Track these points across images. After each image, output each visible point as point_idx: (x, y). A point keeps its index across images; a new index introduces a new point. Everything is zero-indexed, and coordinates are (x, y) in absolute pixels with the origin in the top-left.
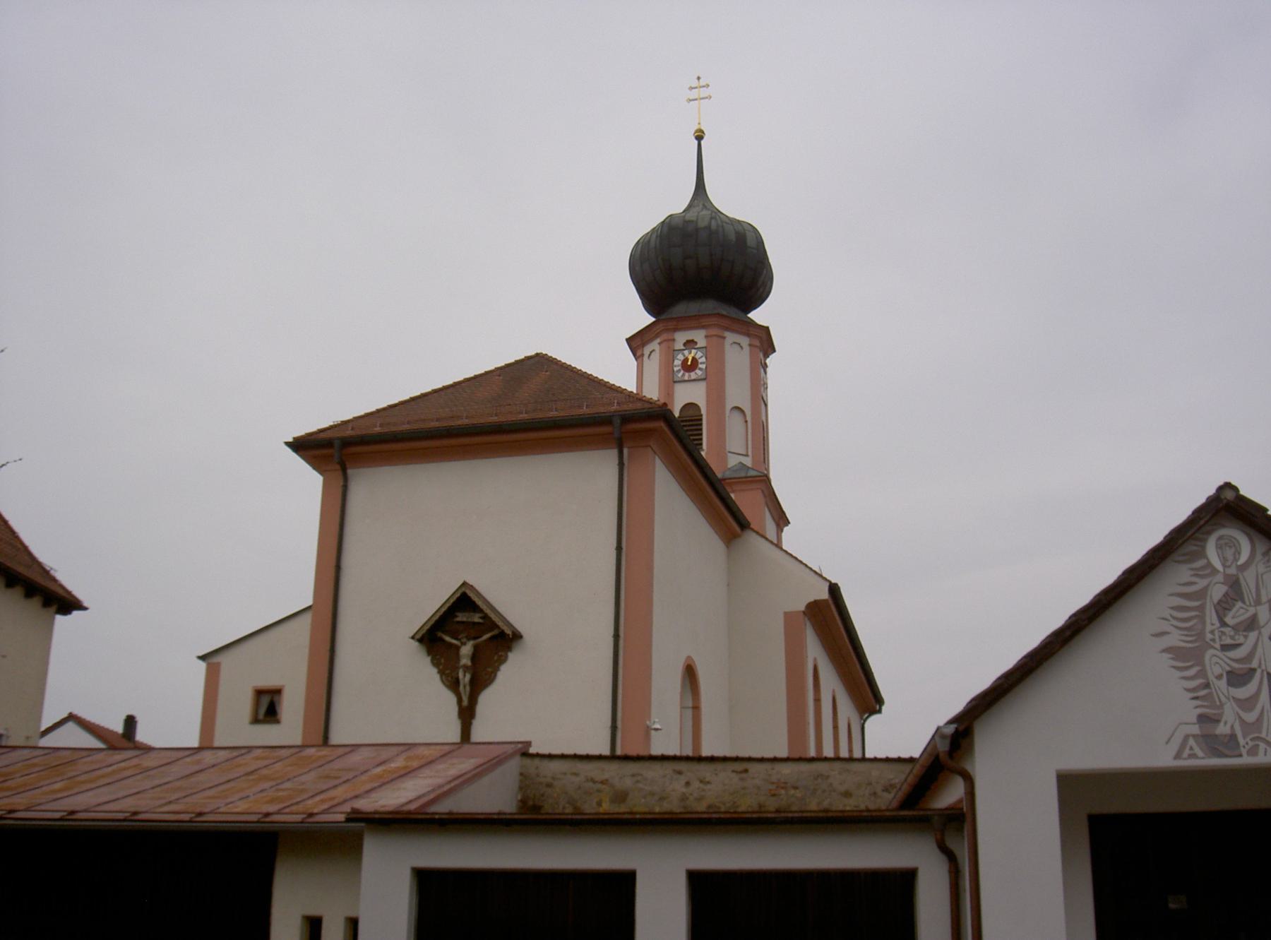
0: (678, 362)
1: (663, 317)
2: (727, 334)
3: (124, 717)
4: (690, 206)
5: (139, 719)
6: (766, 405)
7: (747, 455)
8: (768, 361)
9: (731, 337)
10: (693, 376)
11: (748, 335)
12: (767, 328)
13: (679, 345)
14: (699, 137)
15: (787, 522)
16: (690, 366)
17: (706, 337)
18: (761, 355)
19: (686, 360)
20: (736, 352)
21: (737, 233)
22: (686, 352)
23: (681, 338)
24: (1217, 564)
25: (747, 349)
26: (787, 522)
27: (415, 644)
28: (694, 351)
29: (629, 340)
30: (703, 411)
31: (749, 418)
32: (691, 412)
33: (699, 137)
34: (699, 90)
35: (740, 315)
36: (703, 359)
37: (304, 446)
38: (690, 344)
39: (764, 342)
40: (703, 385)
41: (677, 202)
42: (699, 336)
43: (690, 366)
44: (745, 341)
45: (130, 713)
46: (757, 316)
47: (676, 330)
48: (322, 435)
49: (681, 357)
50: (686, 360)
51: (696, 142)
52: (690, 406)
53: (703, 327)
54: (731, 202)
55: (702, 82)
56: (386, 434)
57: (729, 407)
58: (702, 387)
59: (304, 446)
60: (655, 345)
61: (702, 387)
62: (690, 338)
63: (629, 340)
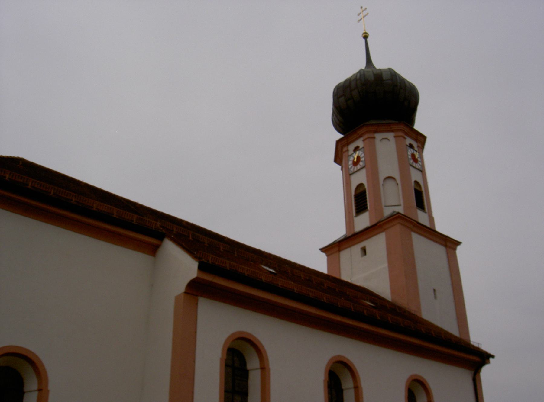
0: (350, 163)
5: (462, 245)
9: (379, 136)
10: (359, 167)
13: (351, 152)
14: (366, 37)
17: (363, 141)
20: (386, 146)
21: (374, 75)
23: (351, 147)
24: (52, 191)
30: (366, 187)
32: (361, 190)
33: (366, 37)
34: (363, 12)
37: (323, 250)
38: (356, 149)
39: (421, 139)
40: (364, 171)
41: (354, 66)
42: (360, 143)
43: (355, 164)
49: (352, 159)
51: (364, 40)
53: (392, 131)
55: (363, 9)
57: (382, 176)
58: (363, 172)
59: (323, 250)
61: (363, 172)
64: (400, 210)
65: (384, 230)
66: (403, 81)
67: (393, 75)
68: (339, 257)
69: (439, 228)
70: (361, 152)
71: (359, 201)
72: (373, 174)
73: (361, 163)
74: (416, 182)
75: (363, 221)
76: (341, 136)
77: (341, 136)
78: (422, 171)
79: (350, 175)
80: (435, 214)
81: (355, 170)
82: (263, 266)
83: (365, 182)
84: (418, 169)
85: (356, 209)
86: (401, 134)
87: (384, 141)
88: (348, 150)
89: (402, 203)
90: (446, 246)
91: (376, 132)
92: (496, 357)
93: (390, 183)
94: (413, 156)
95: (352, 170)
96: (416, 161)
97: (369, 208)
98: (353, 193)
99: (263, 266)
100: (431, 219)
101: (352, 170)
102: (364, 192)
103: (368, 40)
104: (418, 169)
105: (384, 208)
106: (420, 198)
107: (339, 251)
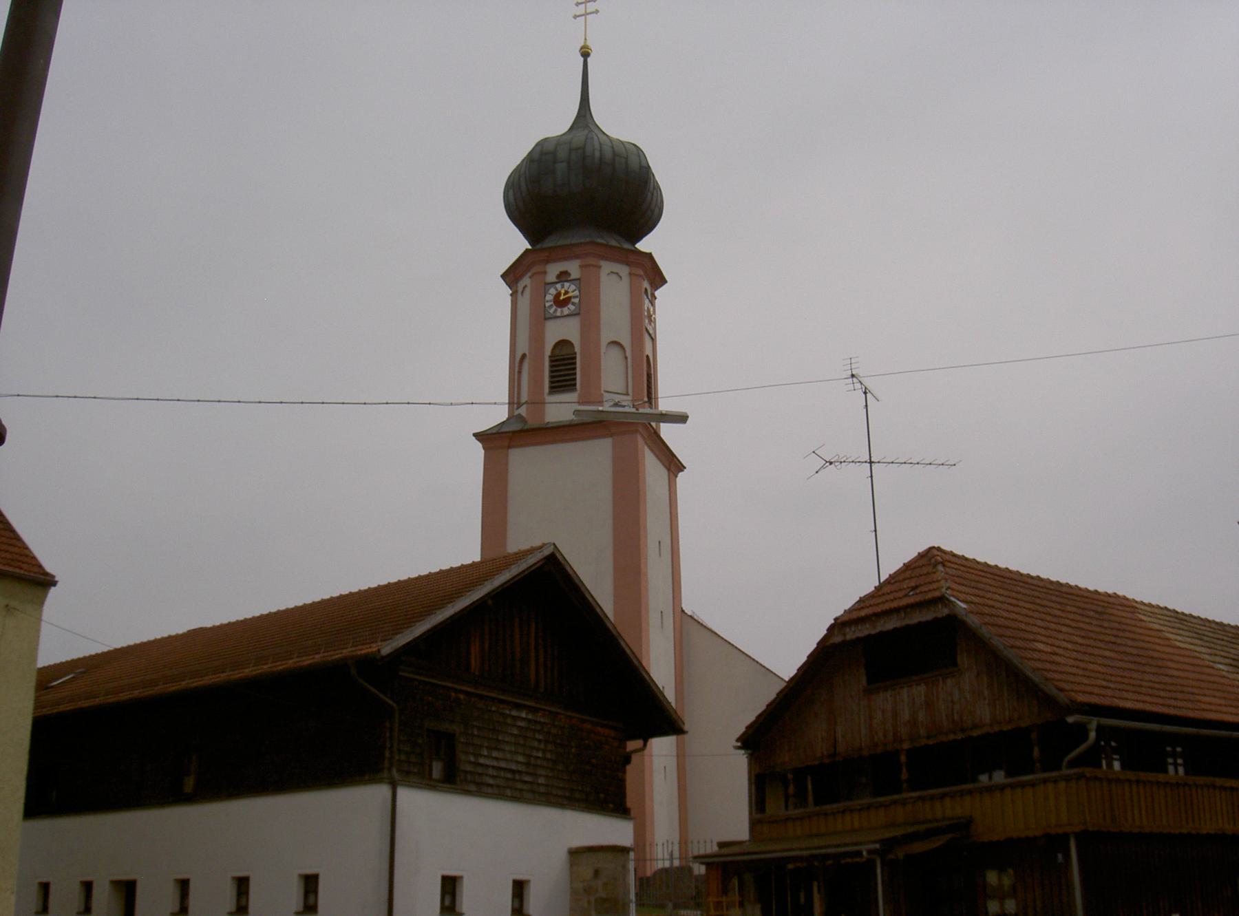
0: (549, 297)
1: (538, 246)
2: (603, 263)
3: (566, 850)
4: (572, 128)
6: (653, 340)
7: (627, 394)
8: (657, 293)
9: (607, 267)
10: (566, 311)
11: (628, 263)
12: (650, 254)
14: (585, 54)
15: (680, 467)
16: (560, 302)
17: (581, 267)
18: (646, 284)
19: (559, 294)
20: (613, 286)
22: (559, 286)
23: (553, 271)
26: (680, 467)
27: (686, 728)
28: (566, 285)
29: (504, 276)
30: (577, 349)
31: (629, 354)
33: (585, 54)
35: (627, 246)
36: (577, 293)
37: (479, 436)
38: (563, 276)
41: (556, 122)
42: (574, 268)
43: (560, 302)
44: (624, 270)
46: (643, 245)
47: (548, 261)
49: (553, 291)
50: (559, 294)
52: (563, 344)
53: (577, 257)
54: (617, 123)
59: (479, 436)
60: (526, 281)
61: (574, 323)
63: (504, 276)
65: (611, 435)
68: (507, 455)
71: (563, 370)
73: (572, 307)
75: (561, 408)
79: (546, 319)
81: (558, 314)
82: (809, 778)
87: (614, 276)
88: (545, 273)
90: (669, 470)
93: (615, 353)
95: (552, 311)
97: (578, 386)
98: (548, 352)
99: (809, 778)
101: (552, 311)
107: (509, 447)
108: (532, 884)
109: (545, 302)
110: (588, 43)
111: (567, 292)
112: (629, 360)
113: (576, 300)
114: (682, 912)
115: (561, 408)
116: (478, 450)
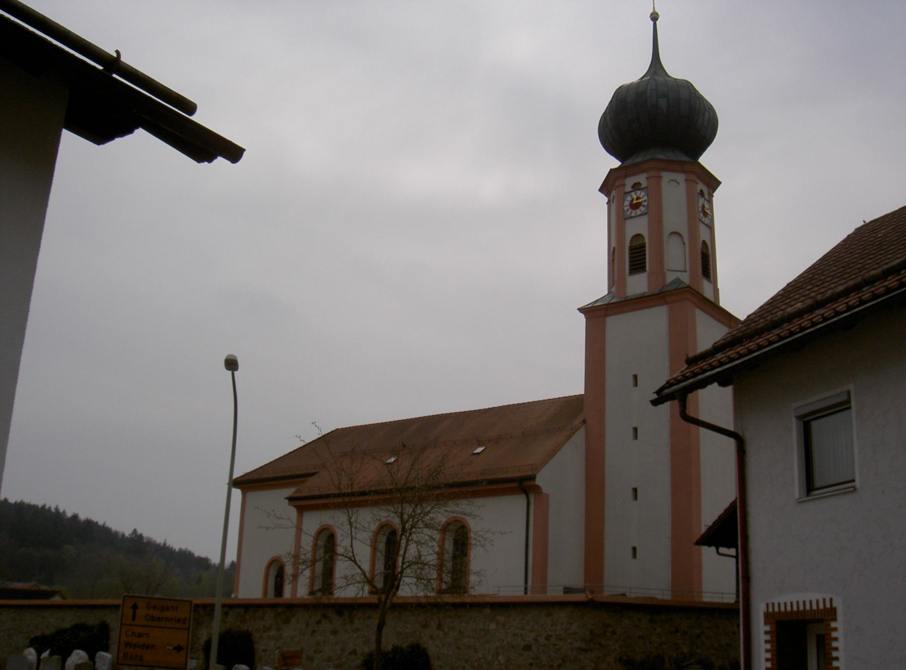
0: (627, 203)
1: (629, 162)
2: (664, 174)
9: (666, 176)
10: (638, 212)
12: (611, 170)
13: (628, 188)
14: (654, 17)
16: (634, 206)
17: (647, 178)
20: (674, 189)
22: (633, 194)
23: (630, 182)
25: (683, 185)
28: (638, 192)
30: (647, 241)
31: (686, 240)
32: (637, 243)
33: (654, 17)
36: (645, 198)
38: (636, 186)
39: (713, 183)
40: (645, 218)
41: (634, 71)
42: (642, 179)
43: (634, 206)
44: (680, 177)
45: (76, 512)
48: (245, 478)
49: (629, 198)
52: (638, 236)
53: (644, 171)
54: (676, 68)
56: (464, 502)
58: (644, 220)
59: (581, 310)
61: (644, 220)
62: (636, 181)
63: (601, 190)
64: (685, 279)
65: (666, 303)
66: (701, 98)
67: (687, 87)
68: (604, 323)
69: (722, 304)
70: (643, 194)
72: (657, 224)
73: (642, 209)
74: (704, 242)
75: (638, 284)
76: (615, 163)
77: (615, 163)
78: (711, 228)
80: (720, 285)
81: (633, 215)
83: (646, 235)
84: (706, 225)
85: (630, 266)
86: (693, 177)
88: (624, 185)
89: (688, 270)
91: (664, 170)
92: (635, 441)
93: (675, 240)
94: (703, 206)
96: (705, 214)
98: (628, 244)
100: (716, 291)
102: (643, 247)
103: (657, 22)
104: (706, 225)
105: (668, 273)
106: (706, 263)
107: (606, 316)
108: (842, 633)
109: (623, 206)
110: (657, 10)
111: (638, 198)
112: (687, 244)
113: (645, 203)
114: (265, 668)
115: (638, 284)
116: (582, 318)
